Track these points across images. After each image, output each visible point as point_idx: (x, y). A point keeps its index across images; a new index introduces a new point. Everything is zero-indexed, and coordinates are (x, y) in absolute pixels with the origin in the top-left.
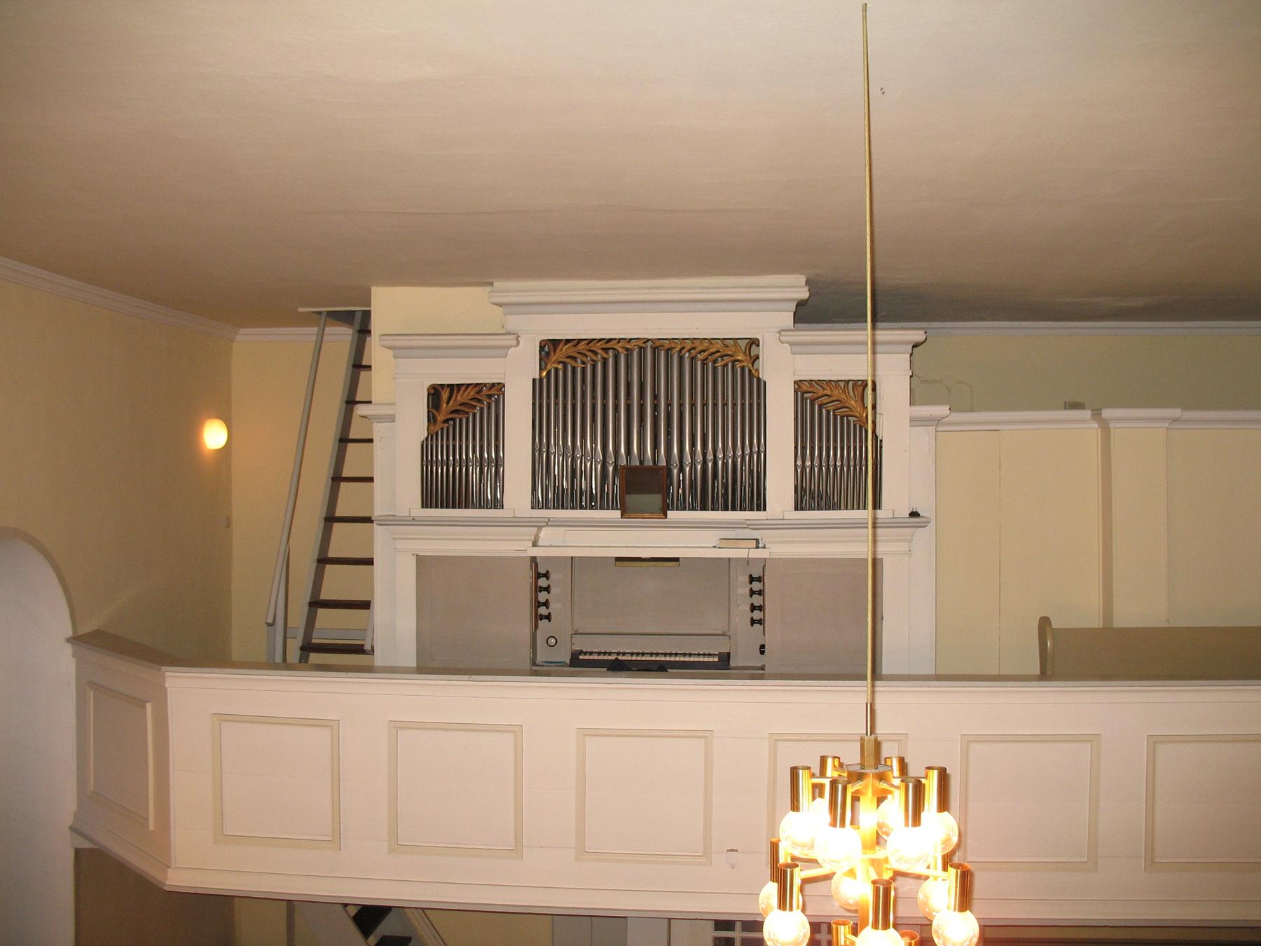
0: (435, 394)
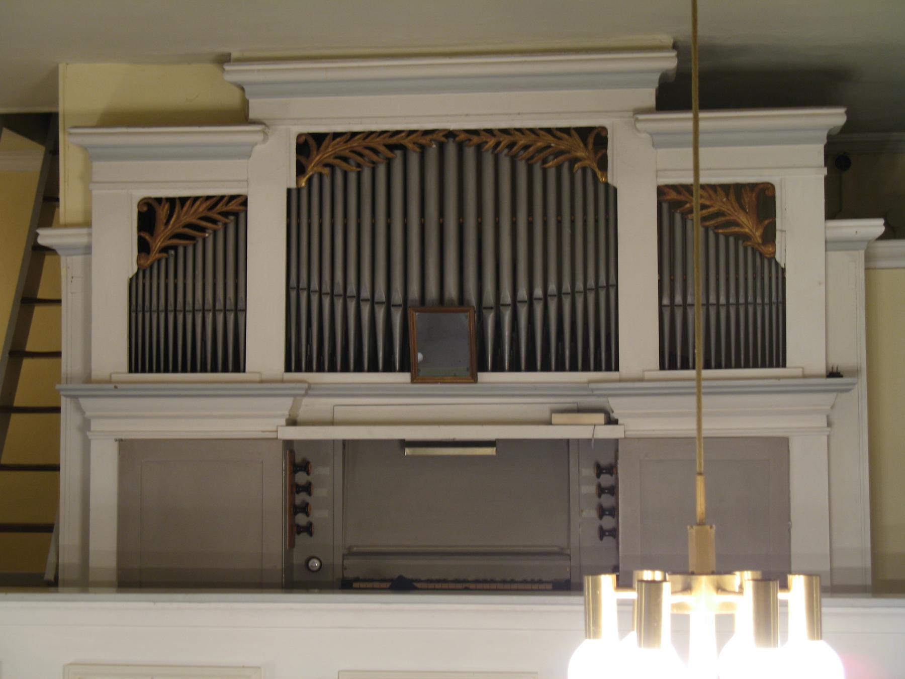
0: (149, 215)
